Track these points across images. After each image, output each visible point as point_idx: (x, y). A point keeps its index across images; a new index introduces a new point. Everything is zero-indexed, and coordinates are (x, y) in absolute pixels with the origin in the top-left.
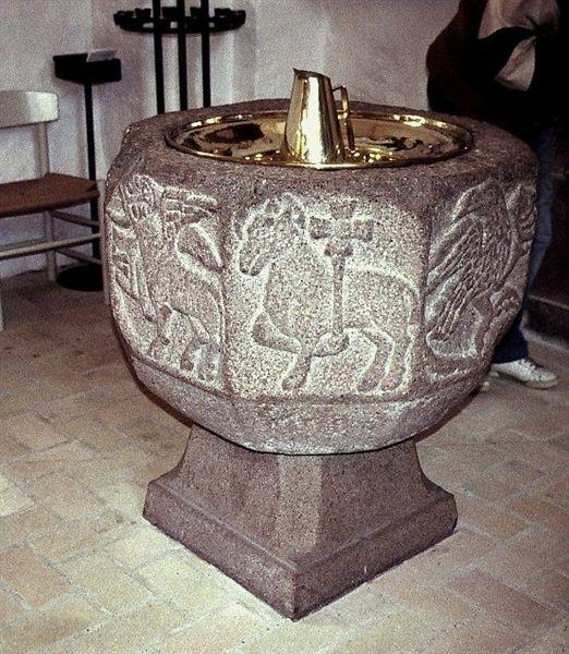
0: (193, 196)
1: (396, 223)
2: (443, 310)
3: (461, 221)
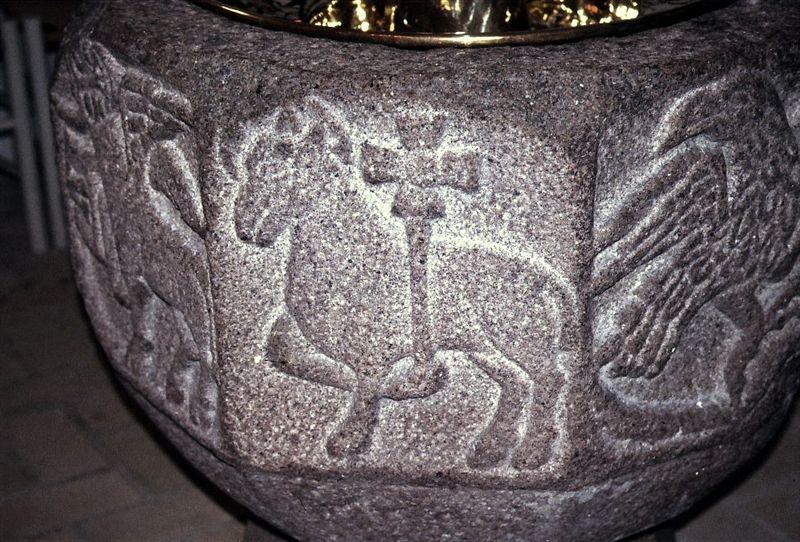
0: (161, 90)
1: (528, 166)
2: (637, 323)
3: (673, 154)
